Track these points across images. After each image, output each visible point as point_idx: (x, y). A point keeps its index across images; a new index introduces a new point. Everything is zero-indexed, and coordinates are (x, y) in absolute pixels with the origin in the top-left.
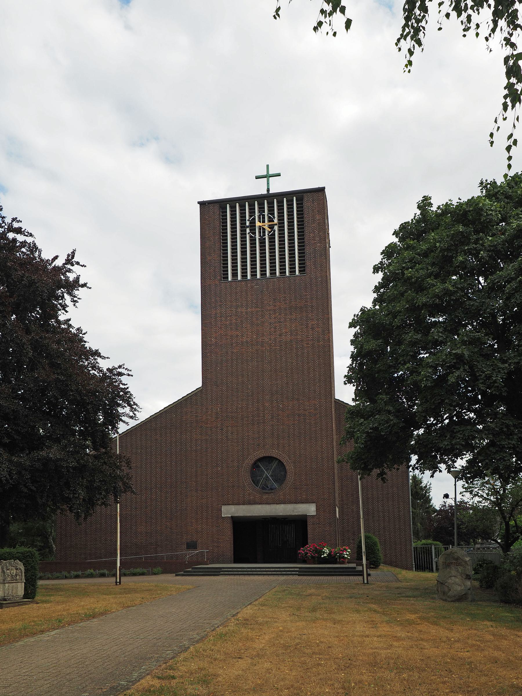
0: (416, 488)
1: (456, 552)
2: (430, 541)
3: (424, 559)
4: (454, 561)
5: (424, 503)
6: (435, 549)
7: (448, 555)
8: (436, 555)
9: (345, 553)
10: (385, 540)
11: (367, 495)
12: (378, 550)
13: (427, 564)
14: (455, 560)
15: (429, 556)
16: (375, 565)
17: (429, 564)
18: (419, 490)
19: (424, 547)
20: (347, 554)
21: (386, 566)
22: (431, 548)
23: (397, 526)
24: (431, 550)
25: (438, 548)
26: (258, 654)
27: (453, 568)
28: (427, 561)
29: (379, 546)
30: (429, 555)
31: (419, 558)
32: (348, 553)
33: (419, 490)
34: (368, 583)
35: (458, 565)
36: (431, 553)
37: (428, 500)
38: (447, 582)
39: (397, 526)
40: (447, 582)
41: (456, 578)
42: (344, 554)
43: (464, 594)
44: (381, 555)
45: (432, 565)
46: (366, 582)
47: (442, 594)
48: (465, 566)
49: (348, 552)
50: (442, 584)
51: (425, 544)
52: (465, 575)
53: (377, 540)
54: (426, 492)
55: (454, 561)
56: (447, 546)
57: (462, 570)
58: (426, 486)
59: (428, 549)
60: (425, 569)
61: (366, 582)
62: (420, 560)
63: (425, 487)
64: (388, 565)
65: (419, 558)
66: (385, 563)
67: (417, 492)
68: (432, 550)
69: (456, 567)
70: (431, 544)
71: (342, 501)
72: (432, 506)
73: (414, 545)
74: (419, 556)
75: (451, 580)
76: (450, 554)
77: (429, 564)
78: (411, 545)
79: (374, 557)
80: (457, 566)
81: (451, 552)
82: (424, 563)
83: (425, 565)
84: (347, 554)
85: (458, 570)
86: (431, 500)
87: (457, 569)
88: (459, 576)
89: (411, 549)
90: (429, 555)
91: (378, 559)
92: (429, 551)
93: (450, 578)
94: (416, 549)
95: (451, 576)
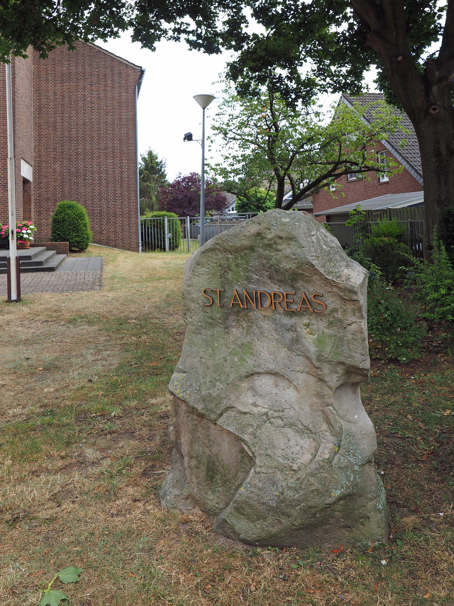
0: (152, 163)
1: (291, 239)
2: (164, 213)
3: (154, 234)
4: (276, 289)
5: (160, 178)
6: (169, 221)
7: (237, 251)
8: (170, 229)
9: (24, 231)
10: (101, 210)
11: (77, 149)
12: (85, 225)
13: (158, 241)
14: (281, 282)
15: (160, 231)
16: (79, 248)
17: (161, 242)
18: (155, 165)
19: (154, 219)
20: (28, 234)
21: (99, 247)
22: (164, 220)
23: (118, 192)
24: (164, 224)
25: (173, 220)
26: (260, 167)
27: (266, 325)
28: (158, 238)
29: (87, 220)
30: (160, 229)
31: (148, 234)
32: (29, 231)
33: (155, 165)
34: (19, 300)
35: (294, 307)
36: (164, 226)
37: (163, 176)
38: (228, 408)
39: (118, 192)
40: (228, 408)
41: (282, 384)
42: (23, 233)
43: (340, 498)
44: (90, 232)
45: (164, 241)
46: (14, 296)
47: (203, 474)
48: (339, 315)
49: (31, 229)
50: (201, 416)
51: (155, 216)
52: (340, 369)
53: (84, 210)
54: (161, 167)
55: (276, 289)
56: (185, 218)
57: (320, 342)
58: (161, 162)
59: (160, 223)
60: (155, 248)
61: (14, 296)
62: (148, 236)
63: (160, 162)
64: (104, 245)
65: (148, 234)
66: (94, 242)
67: (152, 167)
68: (164, 224)
69: (286, 321)
70: (163, 216)
71: (40, 156)
72: (167, 181)
73: (141, 218)
74: (148, 231)
75: (256, 393)
76: (252, 248)
77: (161, 242)
78: (137, 217)
79: (78, 236)
80: (292, 314)
81: (259, 234)
82: (155, 240)
83: (155, 243)
84: (28, 234)
85: (297, 340)
86: (166, 175)
87: (290, 335)
88: (302, 377)
89: (137, 223)
90: (160, 229)
91: (84, 238)
92: (160, 224)
93: (245, 385)
94: (144, 223)
95: (252, 374)
